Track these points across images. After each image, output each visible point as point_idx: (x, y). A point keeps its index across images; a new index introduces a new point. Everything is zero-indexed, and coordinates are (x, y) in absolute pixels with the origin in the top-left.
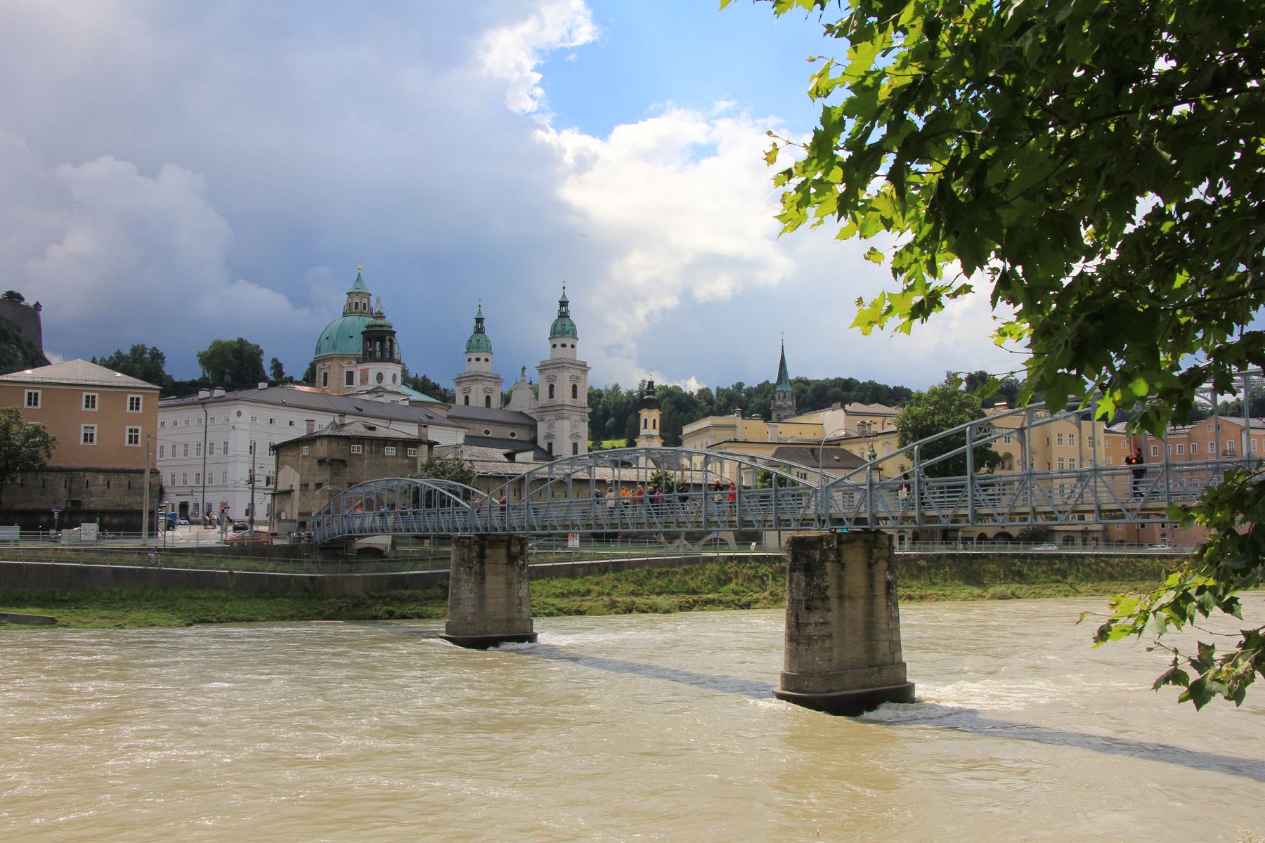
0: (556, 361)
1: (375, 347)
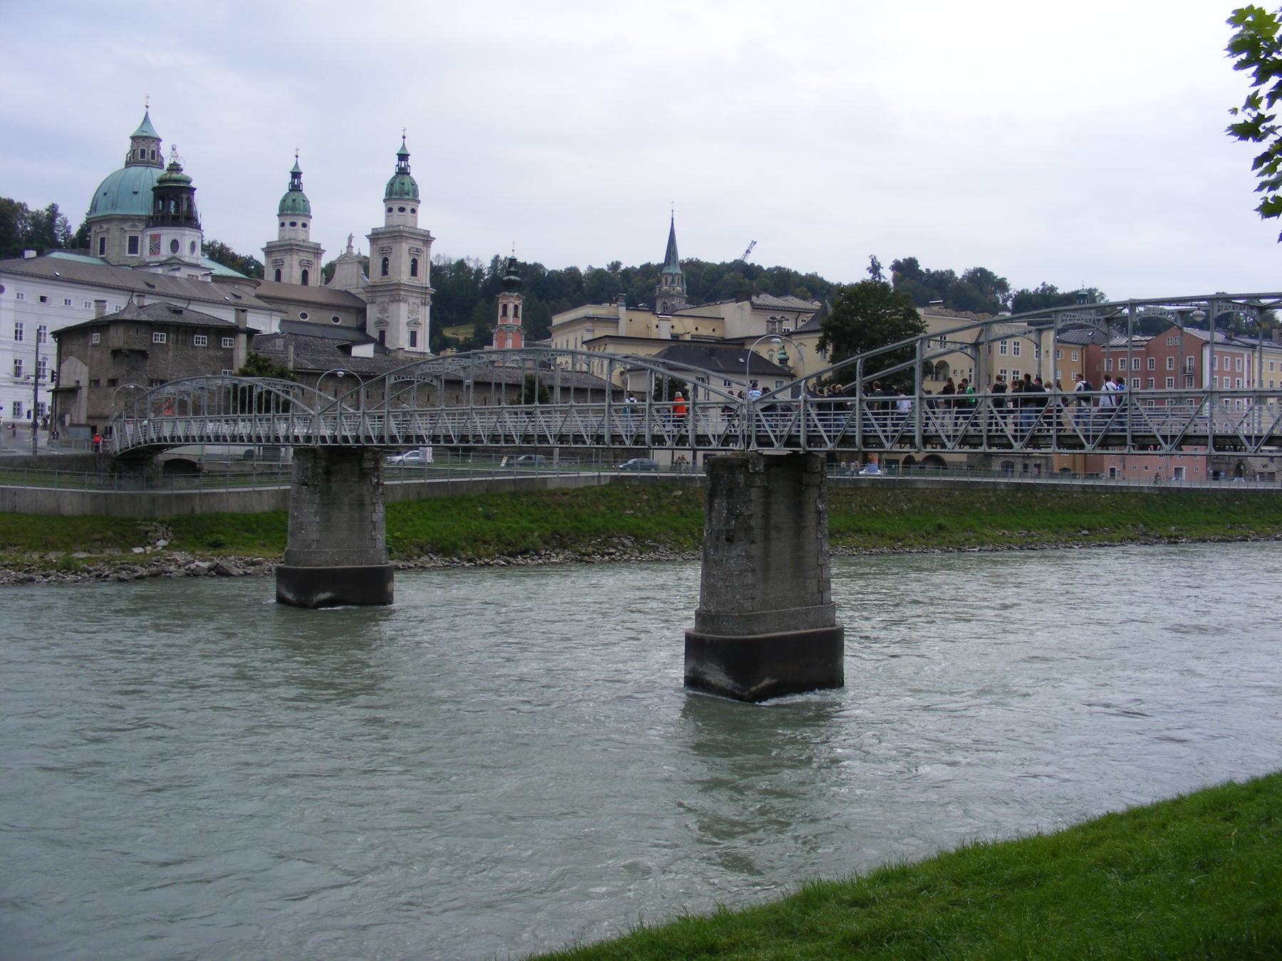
0: (391, 229)
1: (169, 207)
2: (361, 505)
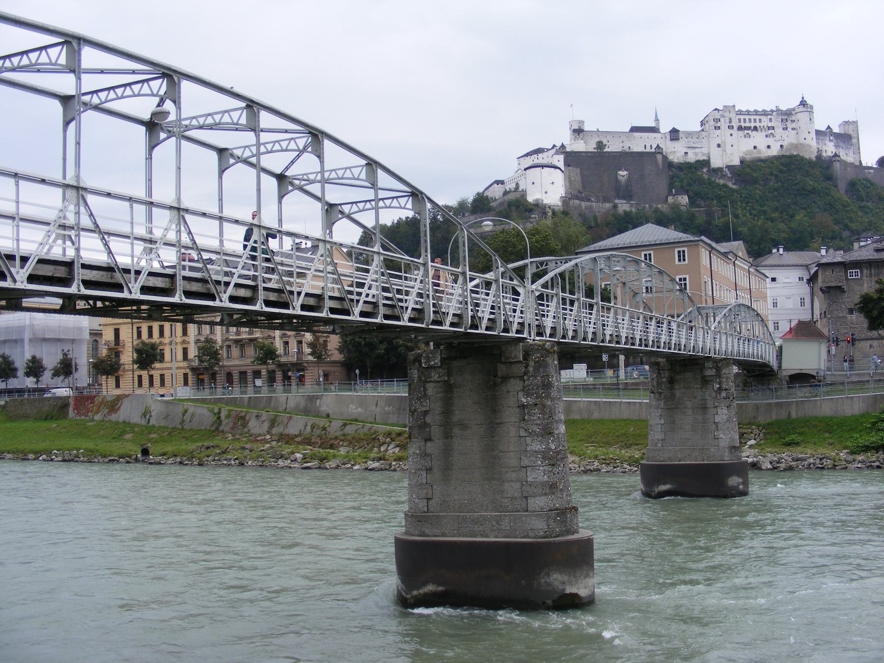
2: (704, 408)
